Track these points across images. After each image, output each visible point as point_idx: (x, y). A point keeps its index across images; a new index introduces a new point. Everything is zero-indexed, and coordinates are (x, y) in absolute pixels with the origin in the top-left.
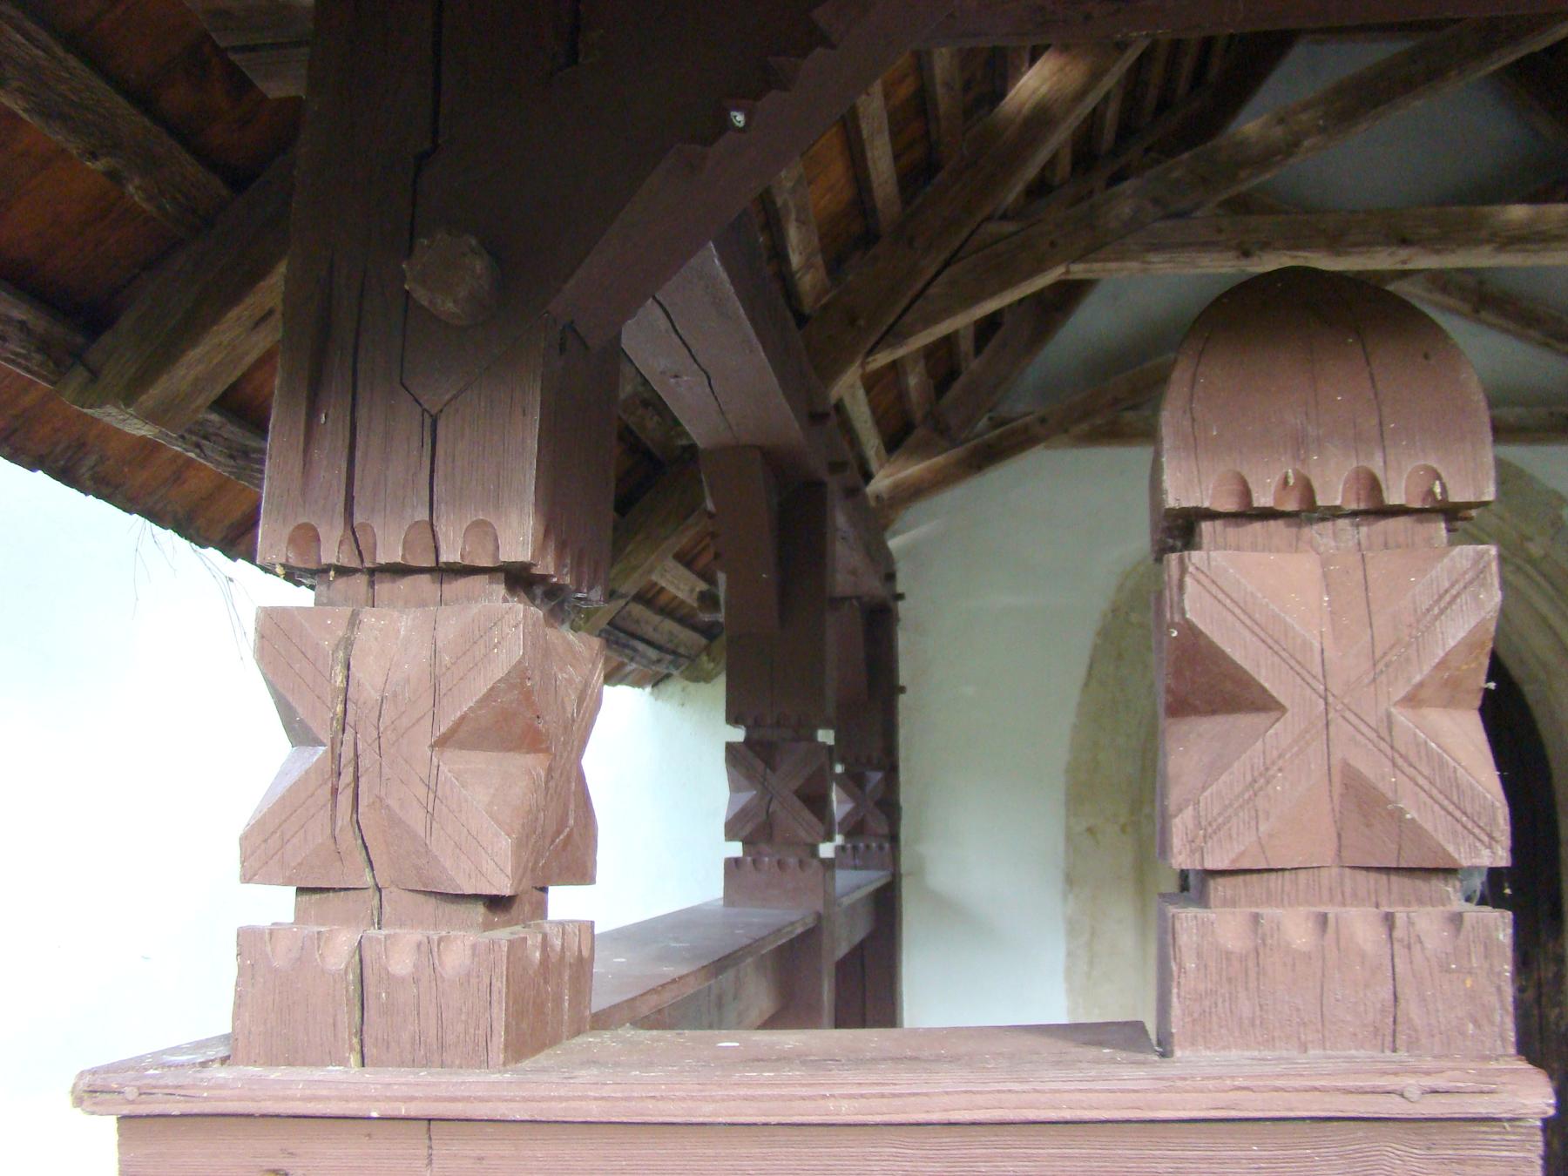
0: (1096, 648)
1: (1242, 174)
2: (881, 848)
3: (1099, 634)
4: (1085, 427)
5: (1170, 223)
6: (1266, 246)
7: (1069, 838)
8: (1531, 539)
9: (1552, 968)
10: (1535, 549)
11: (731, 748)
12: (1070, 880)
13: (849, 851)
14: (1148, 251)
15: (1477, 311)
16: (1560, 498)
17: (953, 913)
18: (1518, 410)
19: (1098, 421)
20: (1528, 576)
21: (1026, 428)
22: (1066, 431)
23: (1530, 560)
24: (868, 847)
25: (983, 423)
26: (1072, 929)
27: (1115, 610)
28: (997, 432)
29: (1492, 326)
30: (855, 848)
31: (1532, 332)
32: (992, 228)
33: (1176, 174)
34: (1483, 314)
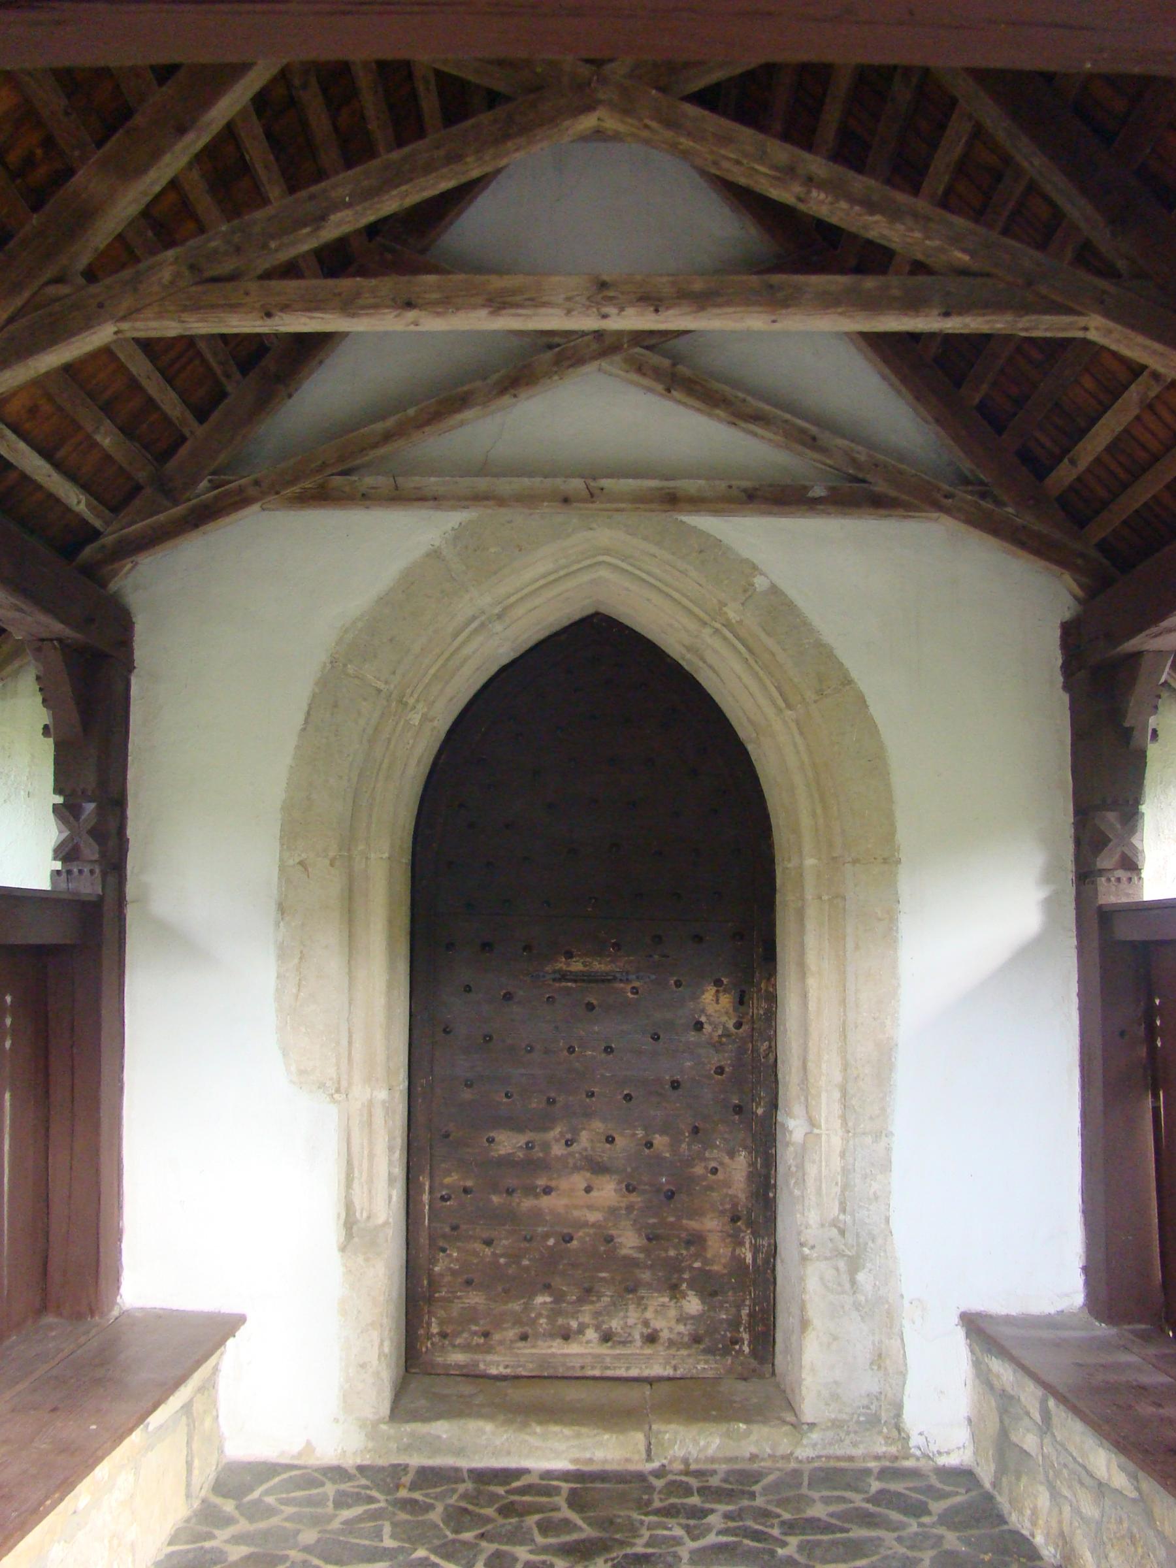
0: (314, 695)
1: (273, 245)
2: (92, 872)
3: (316, 684)
4: (296, 489)
5: (200, 288)
6: (285, 308)
7: (282, 869)
8: (726, 605)
9: (764, 1005)
10: (732, 614)
11: (56, 808)
12: (282, 909)
13: (64, 875)
14: (183, 311)
15: (669, 391)
16: (754, 567)
17: (177, 941)
18: (702, 482)
19: (308, 484)
20: (725, 639)
21: (241, 490)
22: (277, 493)
23: (728, 625)
24: (80, 872)
25: (204, 484)
26: (283, 954)
27: (333, 661)
28: (216, 492)
29: (679, 402)
30: (69, 872)
31: (718, 412)
32: (52, 290)
33: (213, 244)
34: (674, 393)
